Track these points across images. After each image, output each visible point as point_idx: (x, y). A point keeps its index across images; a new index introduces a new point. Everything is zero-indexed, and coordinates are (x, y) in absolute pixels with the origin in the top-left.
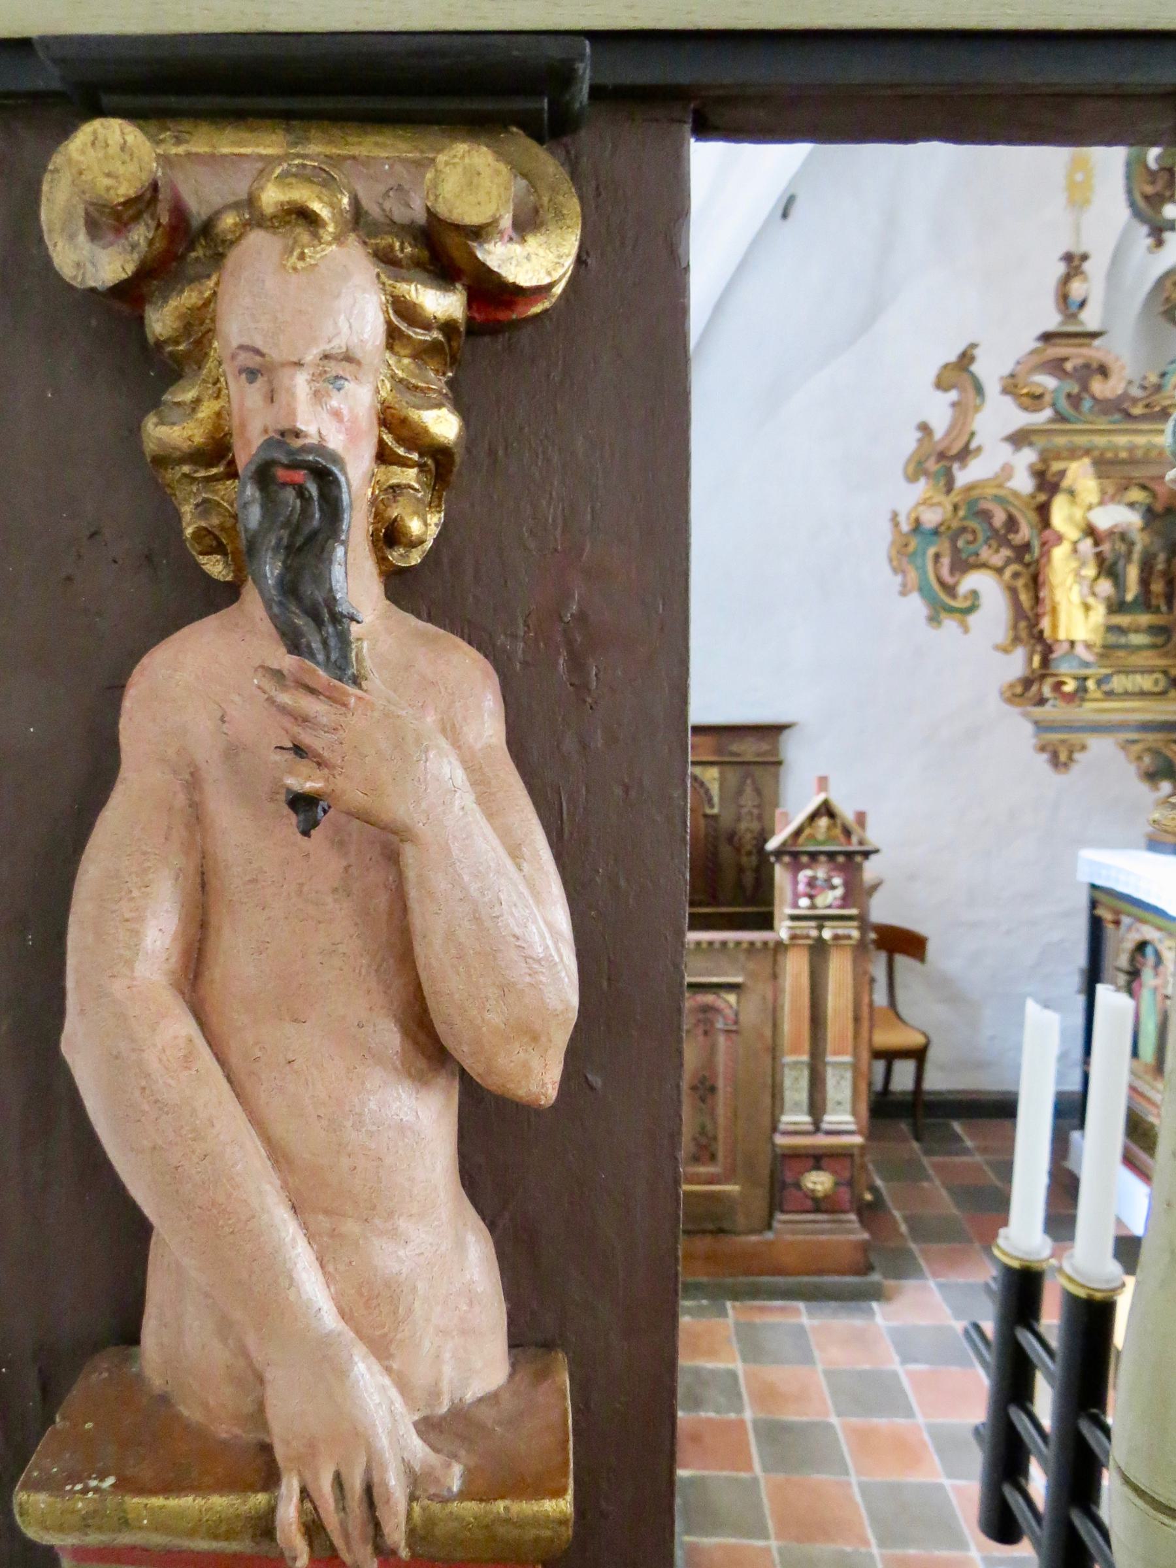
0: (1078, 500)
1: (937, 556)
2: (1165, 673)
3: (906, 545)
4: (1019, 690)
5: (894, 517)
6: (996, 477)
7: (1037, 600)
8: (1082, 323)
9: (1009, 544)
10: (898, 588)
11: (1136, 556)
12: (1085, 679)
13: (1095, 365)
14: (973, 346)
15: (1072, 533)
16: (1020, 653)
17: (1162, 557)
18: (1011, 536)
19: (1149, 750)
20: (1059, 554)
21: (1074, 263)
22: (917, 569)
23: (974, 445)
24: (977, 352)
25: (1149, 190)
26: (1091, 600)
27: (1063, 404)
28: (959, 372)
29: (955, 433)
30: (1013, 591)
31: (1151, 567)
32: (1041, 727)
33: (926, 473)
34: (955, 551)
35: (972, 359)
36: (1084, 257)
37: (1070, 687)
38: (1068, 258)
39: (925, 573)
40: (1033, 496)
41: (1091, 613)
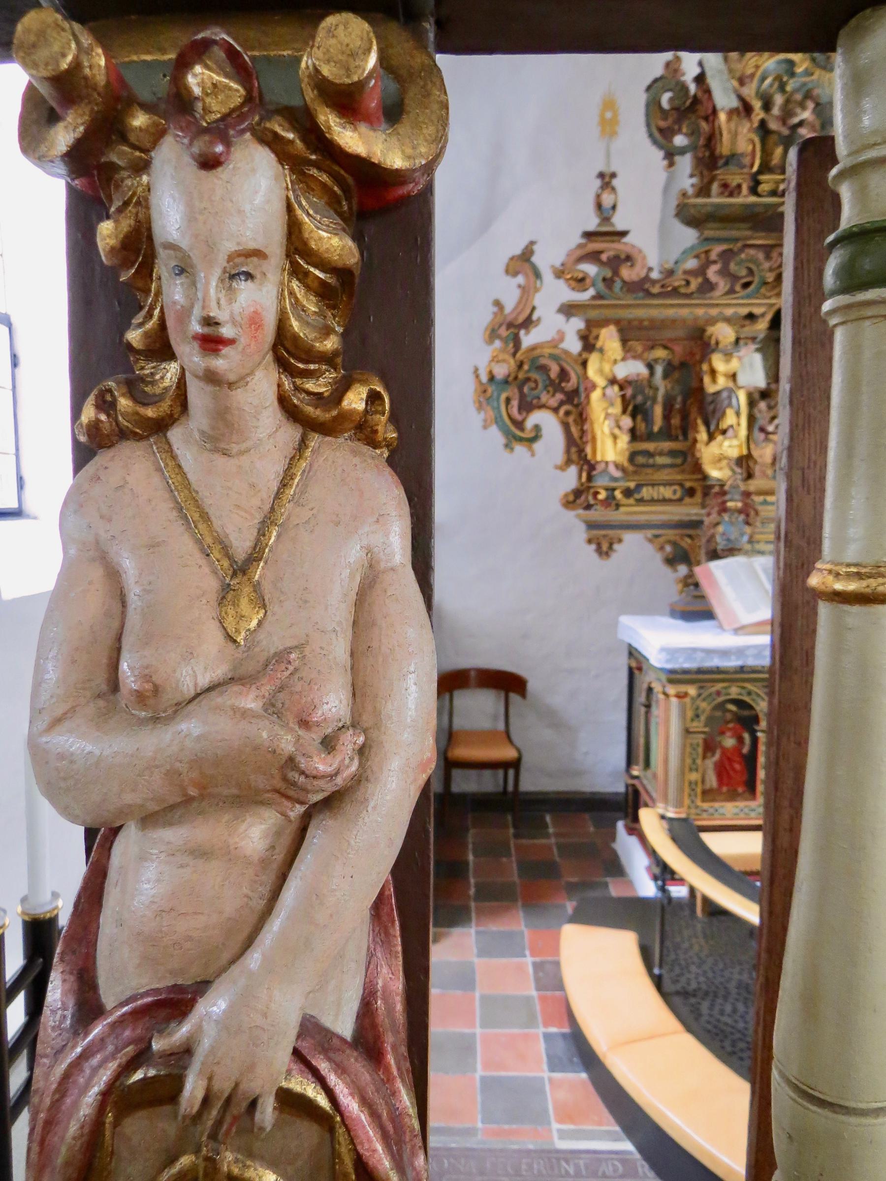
0: (606, 357)
1: (508, 401)
2: (681, 485)
3: (485, 391)
4: (571, 498)
5: (476, 370)
6: (553, 340)
7: (583, 432)
8: (612, 225)
9: (562, 391)
10: (481, 424)
11: (660, 398)
12: (614, 489)
13: (623, 256)
14: (532, 243)
15: (601, 382)
16: (573, 470)
17: (679, 399)
18: (563, 385)
19: (669, 542)
20: (595, 395)
21: (607, 179)
22: (493, 408)
23: (535, 317)
24: (535, 247)
25: (663, 124)
26: (617, 431)
27: (601, 285)
28: (523, 262)
29: (521, 307)
30: (566, 426)
31: (672, 406)
32: (591, 525)
33: (499, 337)
34: (522, 396)
35: (532, 253)
36: (613, 175)
37: (602, 495)
38: (601, 175)
39: (499, 412)
40: (580, 355)
41: (618, 441)
